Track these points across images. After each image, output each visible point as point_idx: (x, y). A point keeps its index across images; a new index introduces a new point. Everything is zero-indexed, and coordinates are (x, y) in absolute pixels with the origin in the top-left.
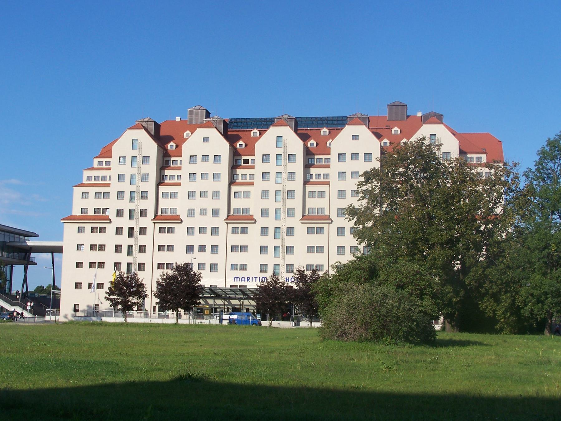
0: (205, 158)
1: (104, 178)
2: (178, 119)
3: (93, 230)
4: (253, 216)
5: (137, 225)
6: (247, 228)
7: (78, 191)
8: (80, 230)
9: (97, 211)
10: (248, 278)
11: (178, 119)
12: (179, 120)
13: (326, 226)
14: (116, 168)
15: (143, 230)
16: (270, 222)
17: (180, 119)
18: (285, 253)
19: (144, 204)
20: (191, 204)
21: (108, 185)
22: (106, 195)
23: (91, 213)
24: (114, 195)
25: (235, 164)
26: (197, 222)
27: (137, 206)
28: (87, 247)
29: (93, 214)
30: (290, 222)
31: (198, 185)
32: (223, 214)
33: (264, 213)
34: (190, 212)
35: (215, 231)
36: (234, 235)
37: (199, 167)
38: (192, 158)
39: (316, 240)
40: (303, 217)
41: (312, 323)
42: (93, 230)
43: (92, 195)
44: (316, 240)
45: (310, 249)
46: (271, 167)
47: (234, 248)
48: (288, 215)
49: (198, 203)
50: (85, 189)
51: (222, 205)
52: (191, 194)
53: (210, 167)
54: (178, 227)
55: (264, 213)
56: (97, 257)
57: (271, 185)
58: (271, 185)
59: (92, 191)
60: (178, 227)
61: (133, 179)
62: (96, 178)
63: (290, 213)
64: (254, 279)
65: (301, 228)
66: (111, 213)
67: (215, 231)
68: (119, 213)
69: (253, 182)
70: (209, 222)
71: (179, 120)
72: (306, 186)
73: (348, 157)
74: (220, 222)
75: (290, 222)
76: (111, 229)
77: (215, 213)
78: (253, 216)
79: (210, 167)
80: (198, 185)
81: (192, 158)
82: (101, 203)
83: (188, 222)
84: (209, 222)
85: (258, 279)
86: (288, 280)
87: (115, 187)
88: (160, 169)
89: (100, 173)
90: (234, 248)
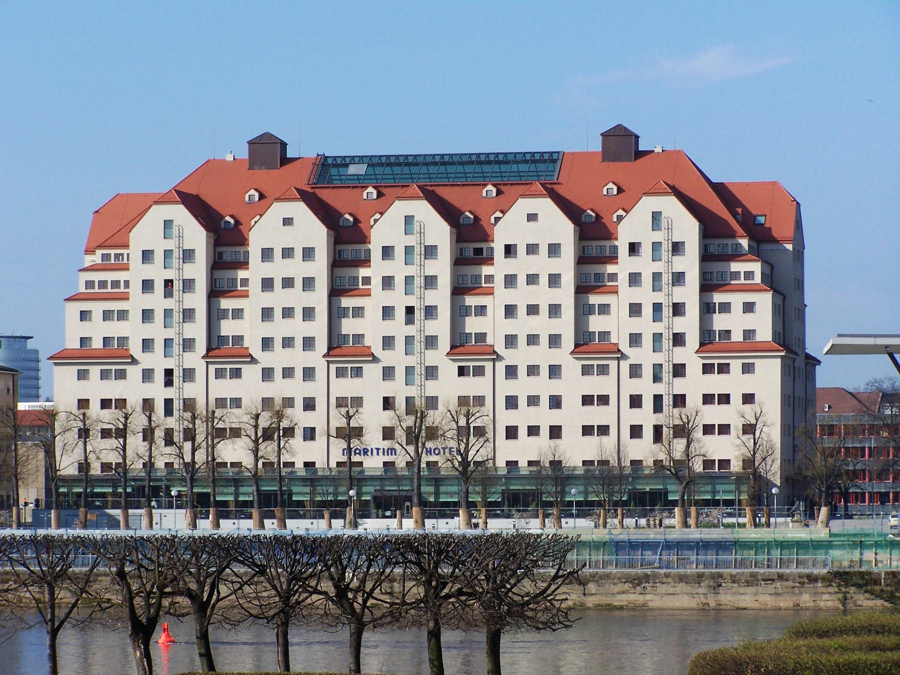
0: (287, 253)
1: (116, 284)
3: (104, 375)
6: (754, 363)
8: (82, 375)
9: (106, 340)
10: (364, 449)
13: (613, 364)
14: (137, 272)
15: (189, 375)
16: (522, 356)
19: (679, 325)
20: (267, 329)
22: (123, 315)
23: (97, 344)
24: (136, 315)
26: (277, 358)
28: (736, 399)
29: (77, 345)
30: (681, 355)
31: (278, 299)
35: (309, 373)
36: (220, 381)
37: (278, 269)
38: (510, 250)
39: (596, 385)
42: (104, 375)
43: (97, 315)
44: (596, 385)
45: (587, 400)
46: (398, 268)
47: (604, 400)
49: (523, 325)
52: (267, 314)
53: (297, 268)
54: (246, 369)
55: (388, 342)
56: (597, 415)
58: (646, 296)
59: (97, 308)
60: (131, 370)
62: (103, 284)
64: (375, 451)
65: (572, 366)
66: (135, 348)
67: (309, 373)
68: (147, 345)
70: (298, 358)
73: (278, 254)
74: (563, 355)
75: (681, 355)
76: (134, 373)
77: (309, 343)
78: (369, 347)
79: (297, 268)
80: (278, 299)
81: (147, 256)
82: (115, 329)
84: (298, 358)
85: (381, 451)
86: (430, 452)
87: (137, 301)
88: (211, 269)
89: (109, 276)
90: (604, 400)
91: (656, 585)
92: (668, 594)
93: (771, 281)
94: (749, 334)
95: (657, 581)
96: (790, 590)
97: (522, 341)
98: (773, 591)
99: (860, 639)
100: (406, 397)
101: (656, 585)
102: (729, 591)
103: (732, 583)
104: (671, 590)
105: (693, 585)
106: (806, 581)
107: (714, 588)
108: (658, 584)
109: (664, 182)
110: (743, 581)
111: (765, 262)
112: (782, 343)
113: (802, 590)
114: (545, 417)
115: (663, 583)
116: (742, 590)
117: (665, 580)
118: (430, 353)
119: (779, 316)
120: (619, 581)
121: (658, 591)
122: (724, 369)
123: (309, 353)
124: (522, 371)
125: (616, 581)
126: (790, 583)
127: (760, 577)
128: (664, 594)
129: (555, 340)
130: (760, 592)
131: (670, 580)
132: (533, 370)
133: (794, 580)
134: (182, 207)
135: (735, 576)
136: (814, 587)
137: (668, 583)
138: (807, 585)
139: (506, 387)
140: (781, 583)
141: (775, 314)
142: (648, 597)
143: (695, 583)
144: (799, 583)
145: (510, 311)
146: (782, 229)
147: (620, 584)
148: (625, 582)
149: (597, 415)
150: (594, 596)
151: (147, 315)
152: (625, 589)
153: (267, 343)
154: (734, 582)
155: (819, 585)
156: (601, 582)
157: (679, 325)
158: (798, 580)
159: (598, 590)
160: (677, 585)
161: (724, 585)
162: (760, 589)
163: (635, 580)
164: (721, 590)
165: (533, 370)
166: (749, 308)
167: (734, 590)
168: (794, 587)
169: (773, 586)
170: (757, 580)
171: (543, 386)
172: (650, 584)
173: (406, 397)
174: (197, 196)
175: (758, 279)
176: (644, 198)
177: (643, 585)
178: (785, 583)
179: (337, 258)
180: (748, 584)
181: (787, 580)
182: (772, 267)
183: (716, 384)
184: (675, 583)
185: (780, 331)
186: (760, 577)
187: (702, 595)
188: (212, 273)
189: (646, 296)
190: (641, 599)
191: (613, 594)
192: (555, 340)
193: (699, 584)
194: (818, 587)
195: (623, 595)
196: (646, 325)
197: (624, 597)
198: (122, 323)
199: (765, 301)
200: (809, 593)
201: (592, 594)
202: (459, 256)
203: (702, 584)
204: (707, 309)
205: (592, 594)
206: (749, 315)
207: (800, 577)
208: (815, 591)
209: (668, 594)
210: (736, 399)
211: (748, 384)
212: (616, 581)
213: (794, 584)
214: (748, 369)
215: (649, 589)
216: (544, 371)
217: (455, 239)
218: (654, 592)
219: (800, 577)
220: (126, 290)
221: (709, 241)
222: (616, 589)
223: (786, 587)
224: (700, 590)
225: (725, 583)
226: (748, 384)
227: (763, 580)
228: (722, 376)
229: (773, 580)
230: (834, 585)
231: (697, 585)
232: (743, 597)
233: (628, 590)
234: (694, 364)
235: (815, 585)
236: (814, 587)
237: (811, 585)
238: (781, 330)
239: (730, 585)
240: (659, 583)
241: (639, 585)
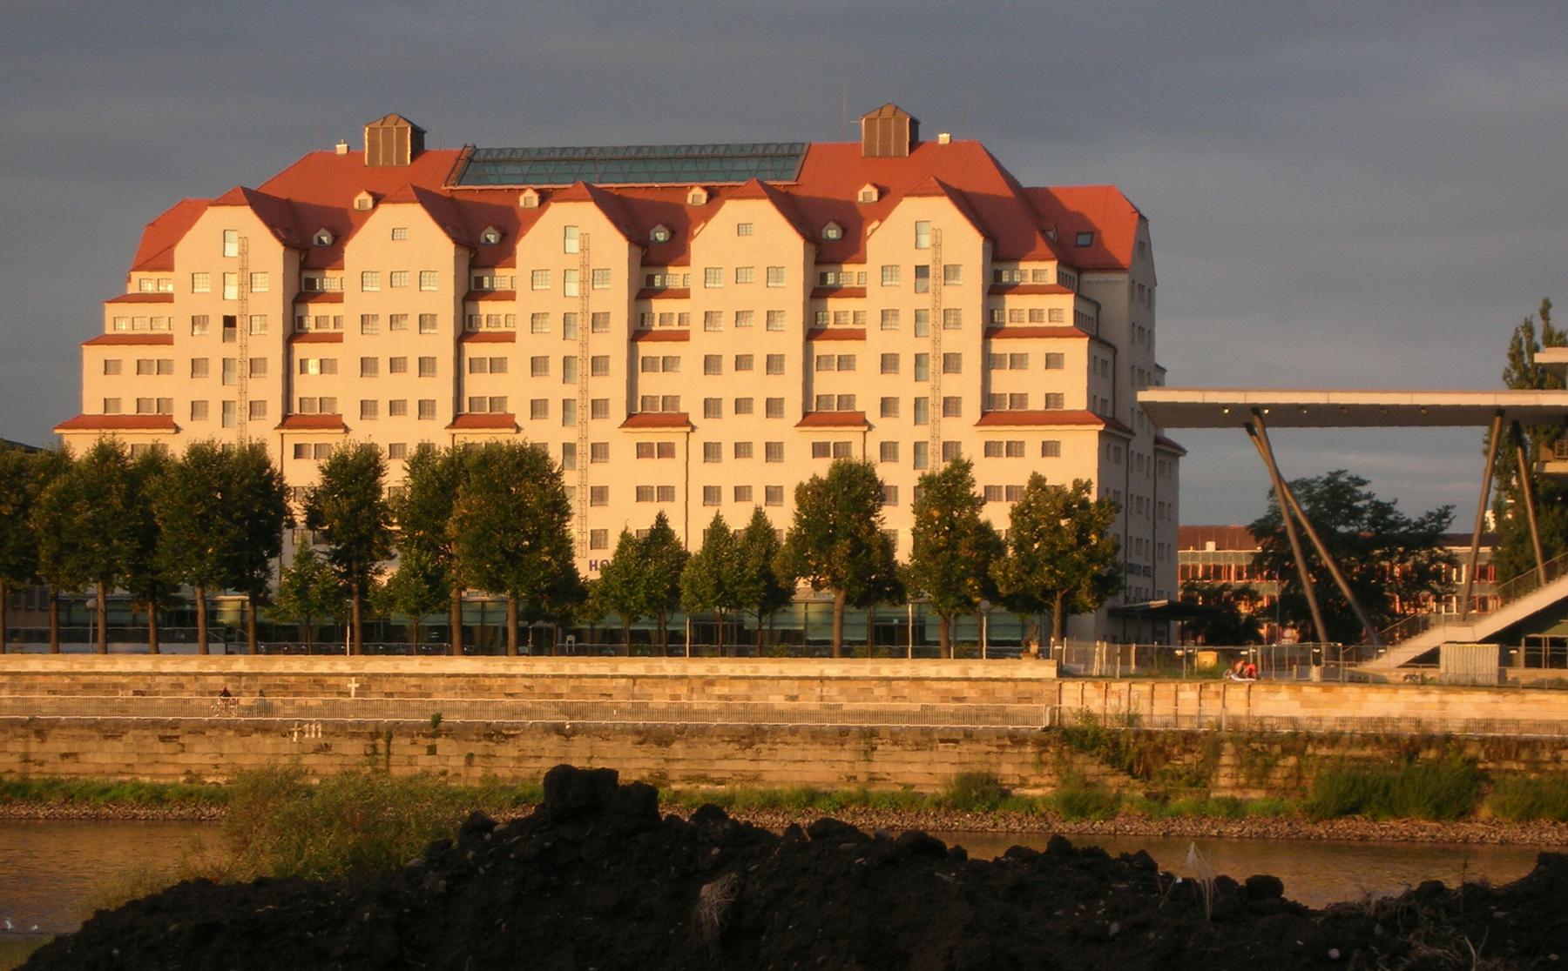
2: (341, 149)
4: (513, 416)
5: (583, 438)
7: (93, 357)
11: (341, 149)
12: (345, 152)
16: (726, 430)
17: (348, 147)
18: (589, 502)
19: (951, 385)
21: (166, 340)
22: (162, 367)
24: (182, 367)
25: (473, 288)
26: (726, 430)
27: (935, 389)
32: (794, 410)
33: (711, 407)
34: (711, 407)
40: (804, 417)
41: (928, 639)
43: (129, 367)
44: (656, 472)
48: (946, 412)
49: (729, 385)
51: (789, 387)
59: (129, 355)
61: (921, 321)
63: (599, 408)
65: (623, 443)
69: (341, 335)
70: (757, 428)
71: (947, 141)
72: (639, 343)
82: (153, 387)
83: (708, 430)
84: (757, 428)
91: (776, 747)
92: (795, 761)
93: (1089, 323)
94: (1052, 399)
95: (778, 740)
96: (984, 758)
97: (728, 407)
98: (956, 760)
99: (1086, 825)
100: (735, 487)
101: (776, 747)
102: (888, 758)
103: (893, 745)
104: (799, 755)
105: (832, 747)
106: (1009, 743)
107: (866, 751)
108: (779, 746)
109: (937, 179)
110: (910, 742)
111: (1079, 296)
112: (1109, 414)
113: (1003, 758)
115: (787, 744)
116: (907, 756)
117: (789, 739)
118: (949, 422)
119: (1104, 375)
120: (720, 739)
121: (778, 758)
123: (773, 422)
124: (728, 451)
125: (715, 739)
126: (983, 747)
127: (936, 736)
128: (789, 761)
129: (773, 407)
130: (936, 760)
131: (798, 739)
132: (742, 450)
133: (988, 740)
134: (247, 211)
135: (897, 734)
136: (1020, 753)
137: (795, 744)
138: (1008, 750)
139: (705, 474)
140: (970, 747)
141: (1095, 369)
142: (763, 766)
143: (836, 744)
144: (998, 746)
145: (367, 366)
146: (1119, 246)
147: (721, 745)
148: (729, 742)
150: (681, 763)
151: (197, 367)
152: (729, 752)
153: (367, 408)
154: (896, 743)
155: (1029, 749)
156: (692, 740)
157: (951, 385)
158: (995, 742)
159: (688, 754)
160: (808, 747)
161: (880, 747)
162: (935, 755)
163: (743, 737)
164: (876, 756)
165: (742, 450)
166: (1053, 361)
167: (896, 757)
168: (988, 753)
169: (957, 750)
170: (932, 740)
172: (768, 745)
173: (735, 487)
174: (288, 201)
175: (1068, 320)
176: (905, 199)
177: (755, 747)
178: (975, 747)
179: (473, 288)
180: (918, 746)
181: (978, 741)
182: (1098, 307)
184: (806, 743)
185: (1105, 397)
186: (936, 736)
187: (846, 764)
188: (294, 310)
190: (752, 767)
191: (710, 760)
192: (773, 407)
193: (842, 745)
194: (1026, 753)
195: (726, 762)
196: (904, 387)
197: (726, 765)
198: (497, 376)
199: (1077, 351)
200: (1013, 764)
201: (678, 760)
202: (818, 285)
203: (847, 747)
204: (989, 362)
205: (678, 760)
206: (1053, 373)
207: (998, 738)
208: (1021, 760)
209: (795, 761)
212: (715, 739)
213: (989, 749)
215: (765, 752)
216: (759, 451)
217: (640, 261)
218: (772, 758)
219: (998, 738)
220: (337, 331)
221: (998, 267)
222: (714, 752)
223: (976, 753)
224: (845, 756)
225: (883, 744)
227: (942, 741)
228: (1012, 460)
229: (956, 741)
230: (1051, 750)
231: (839, 747)
232: (910, 768)
233: (733, 755)
235: (1023, 750)
236: (1020, 753)
237: (1016, 751)
238: (1107, 395)
239: (889, 747)
240: (782, 743)
241: (750, 746)
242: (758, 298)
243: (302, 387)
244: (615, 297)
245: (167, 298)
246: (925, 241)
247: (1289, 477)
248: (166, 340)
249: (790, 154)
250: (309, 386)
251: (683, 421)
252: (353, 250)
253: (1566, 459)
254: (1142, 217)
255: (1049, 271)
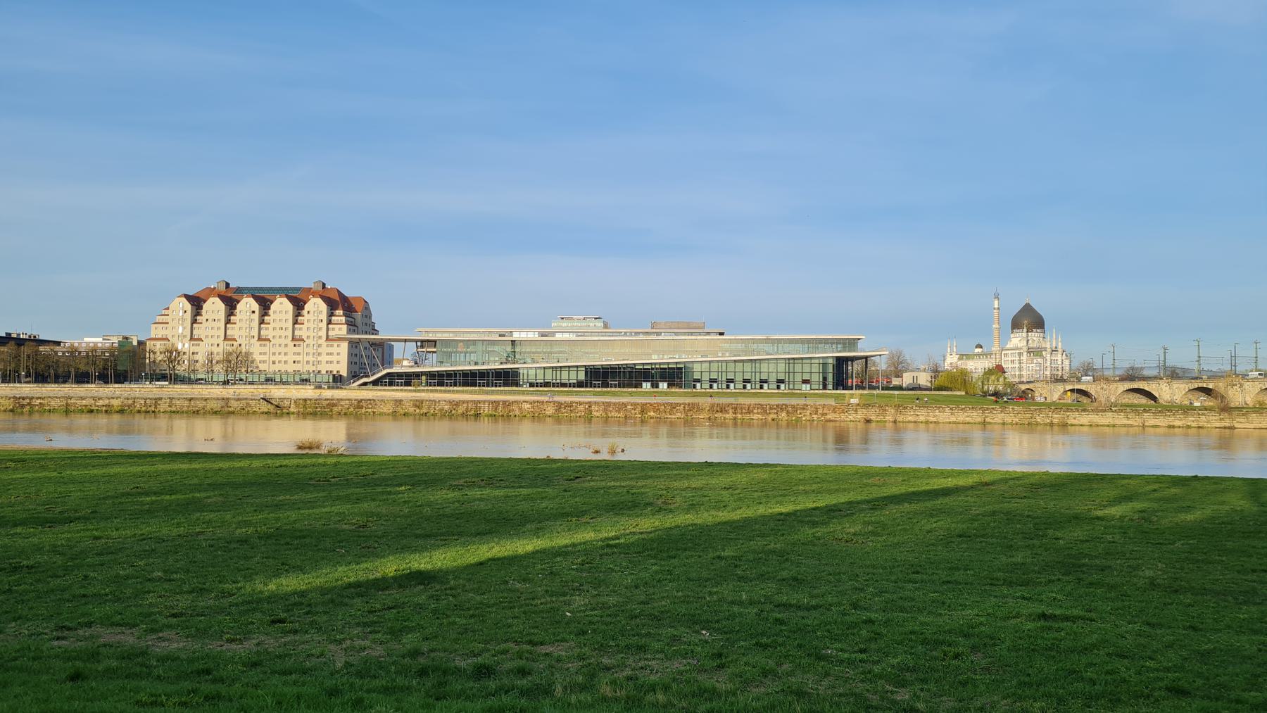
21: (168, 323)
24: (237, 329)
26: (277, 341)
28: (335, 354)
30: (320, 342)
50: (341, 326)
56: (329, 358)
57: (311, 325)
67: (286, 345)
84: (283, 341)
114: (284, 358)
122: (332, 346)
134: (320, 299)
149: (329, 358)
157: (320, 333)
166: (340, 329)
171: (283, 350)
175: (344, 322)
183: (330, 350)
189: (311, 325)
204: (294, 329)
210: (335, 354)
211: (338, 350)
214: (338, 346)
226: (338, 350)
234: (324, 344)
242: (283, 316)
243: (262, 333)
244: (324, 316)
245: (168, 315)
246: (248, 306)
247: (1167, 365)
248: (168, 323)
249: (286, 289)
250: (297, 333)
251: (303, 340)
252: (272, 306)
253: (5, 340)
254: (366, 302)
255: (341, 312)
